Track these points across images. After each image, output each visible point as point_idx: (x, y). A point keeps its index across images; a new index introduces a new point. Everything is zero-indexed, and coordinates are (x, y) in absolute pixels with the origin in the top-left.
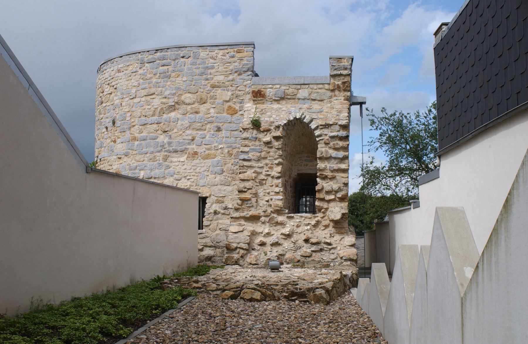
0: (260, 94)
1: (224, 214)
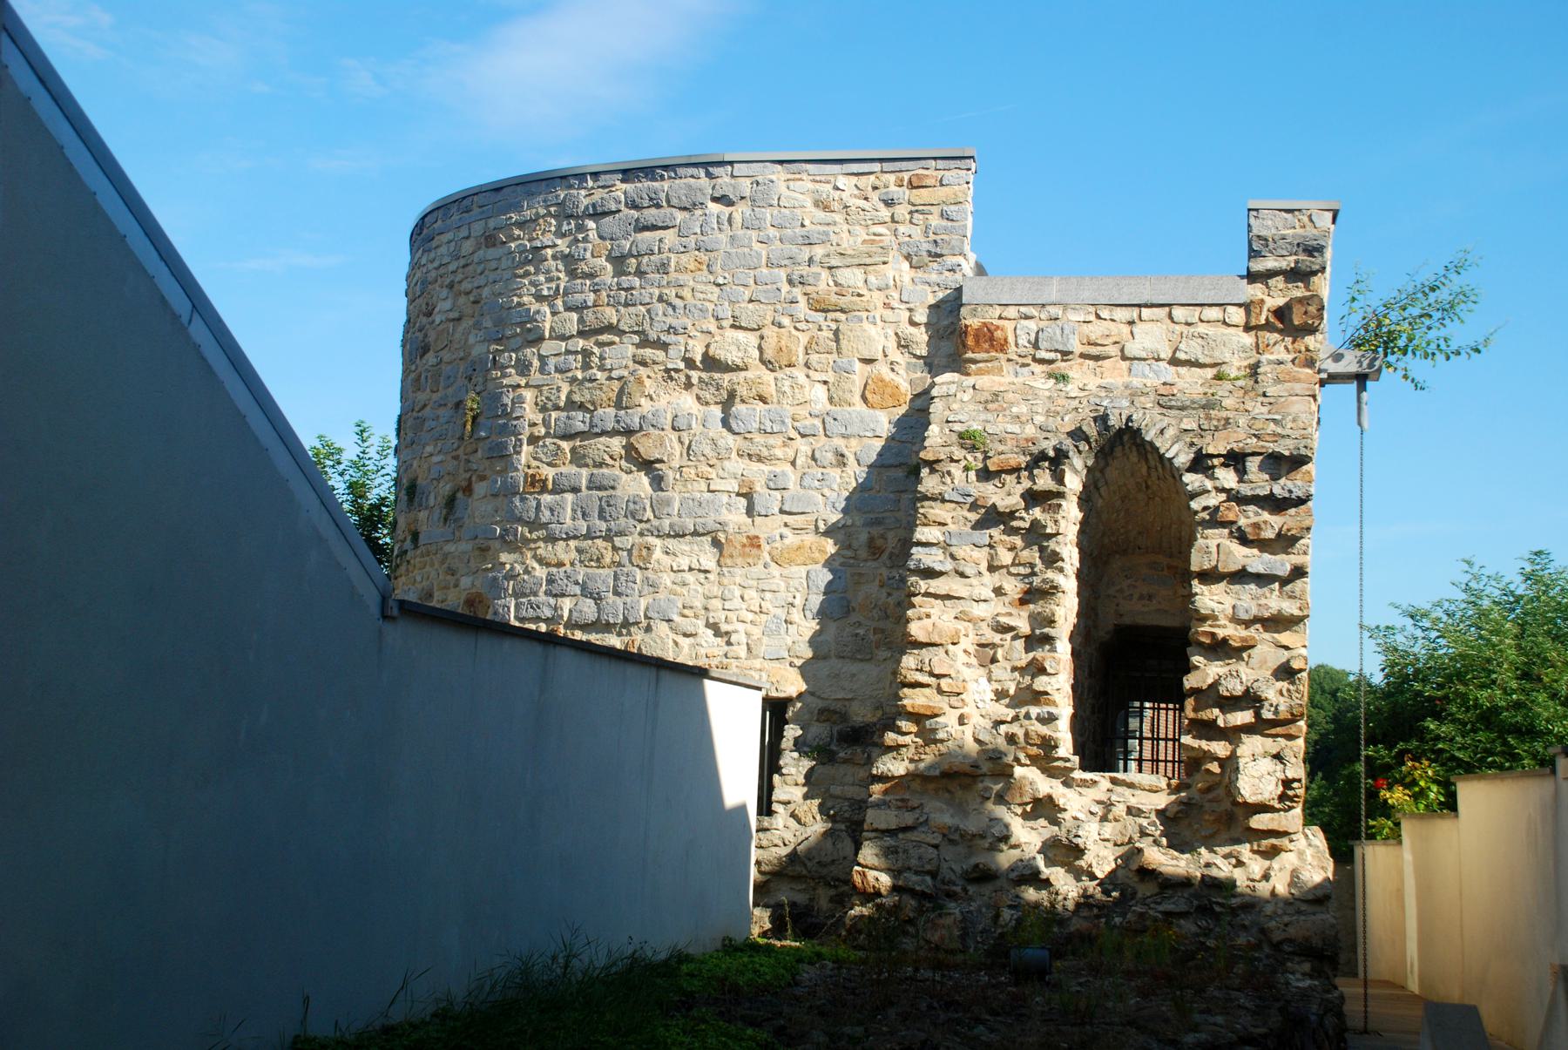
0: (992, 339)
1: (1083, 356)
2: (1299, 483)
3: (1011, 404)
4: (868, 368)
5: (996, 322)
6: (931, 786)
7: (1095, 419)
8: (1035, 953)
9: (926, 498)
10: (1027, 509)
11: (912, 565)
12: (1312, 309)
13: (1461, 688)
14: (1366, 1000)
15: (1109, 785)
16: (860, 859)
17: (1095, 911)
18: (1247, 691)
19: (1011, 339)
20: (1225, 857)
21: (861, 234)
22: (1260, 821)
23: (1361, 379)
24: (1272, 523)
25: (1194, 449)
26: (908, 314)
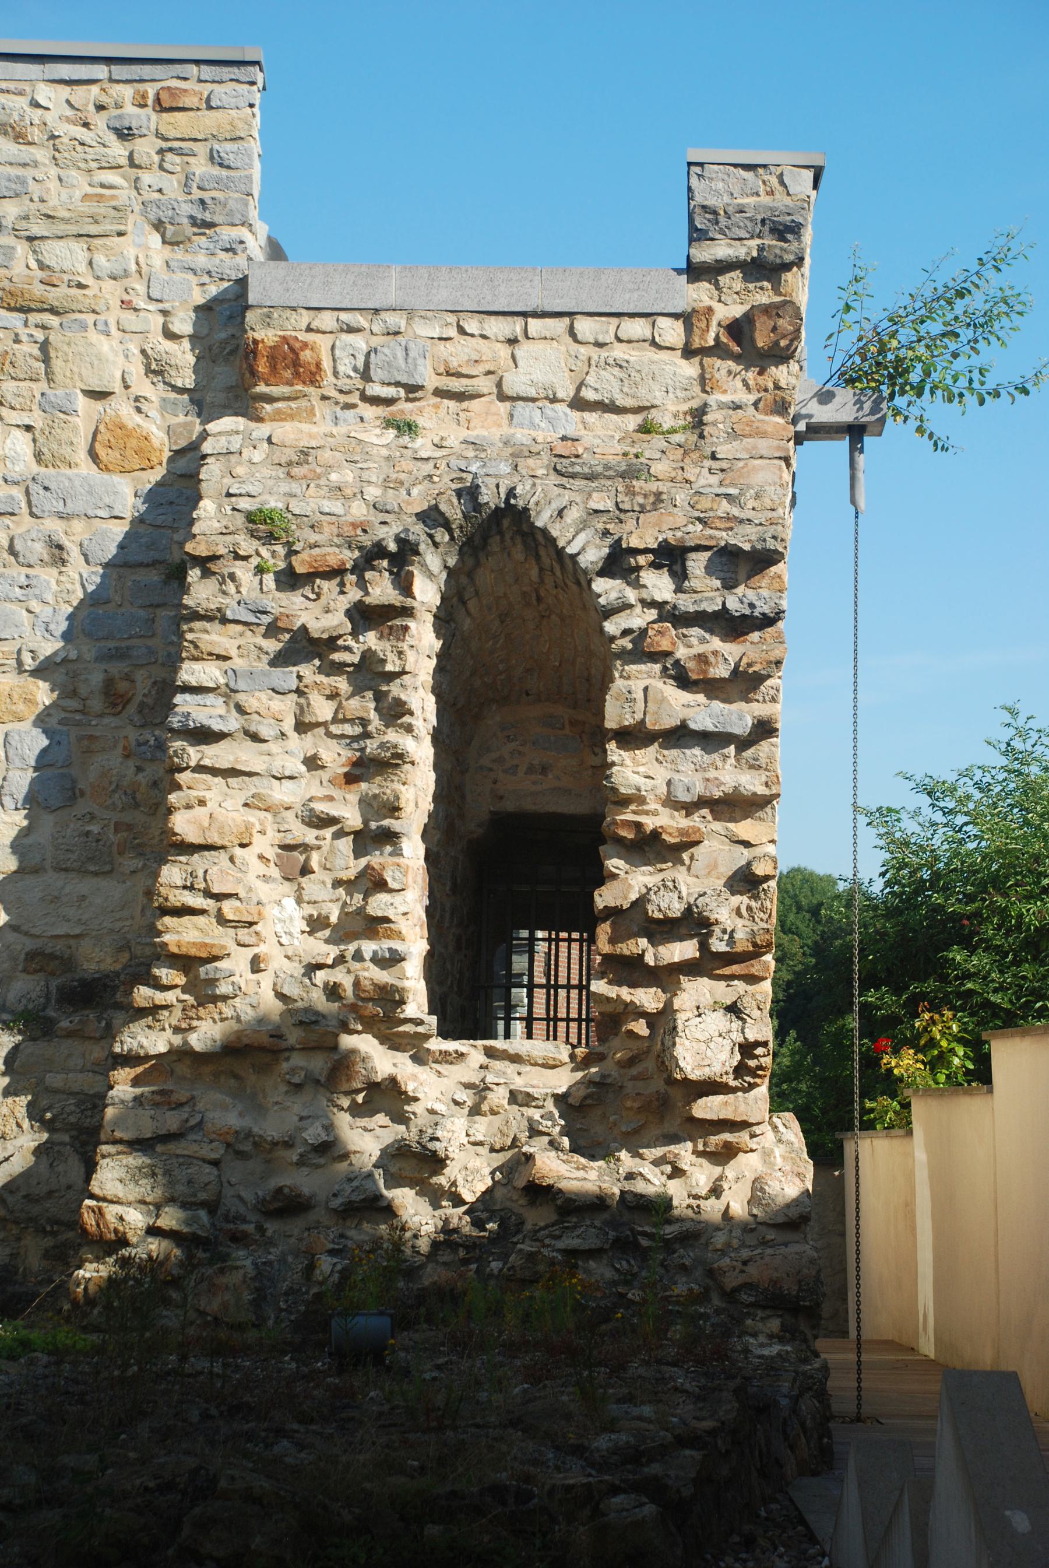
0: (296, 363)
1: (439, 393)
2: (764, 592)
3: (329, 467)
4: (99, 405)
5: (303, 336)
6: (207, 1070)
7: (459, 493)
8: (370, 1323)
9: (196, 616)
10: (355, 634)
11: (175, 721)
12: (784, 324)
13: (1000, 901)
14: (859, 1343)
15: (483, 1059)
16: (95, 1187)
17: (462, 1253)
18: (689, 910)
19: (327, 365)
20: (656, 1163)
21: (81, 184)
22: (707, 1108)
23: (855, 433)
24: (727, 655)
25: (609, 541)
26: (161, 320)
